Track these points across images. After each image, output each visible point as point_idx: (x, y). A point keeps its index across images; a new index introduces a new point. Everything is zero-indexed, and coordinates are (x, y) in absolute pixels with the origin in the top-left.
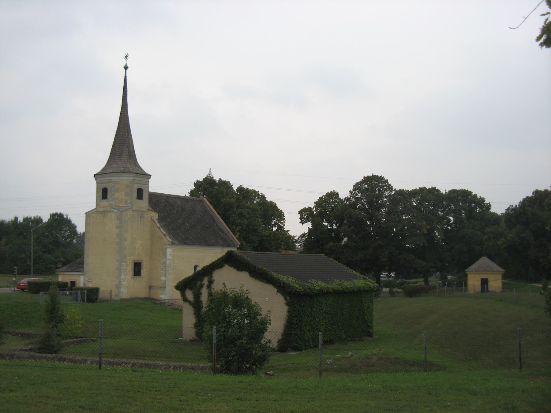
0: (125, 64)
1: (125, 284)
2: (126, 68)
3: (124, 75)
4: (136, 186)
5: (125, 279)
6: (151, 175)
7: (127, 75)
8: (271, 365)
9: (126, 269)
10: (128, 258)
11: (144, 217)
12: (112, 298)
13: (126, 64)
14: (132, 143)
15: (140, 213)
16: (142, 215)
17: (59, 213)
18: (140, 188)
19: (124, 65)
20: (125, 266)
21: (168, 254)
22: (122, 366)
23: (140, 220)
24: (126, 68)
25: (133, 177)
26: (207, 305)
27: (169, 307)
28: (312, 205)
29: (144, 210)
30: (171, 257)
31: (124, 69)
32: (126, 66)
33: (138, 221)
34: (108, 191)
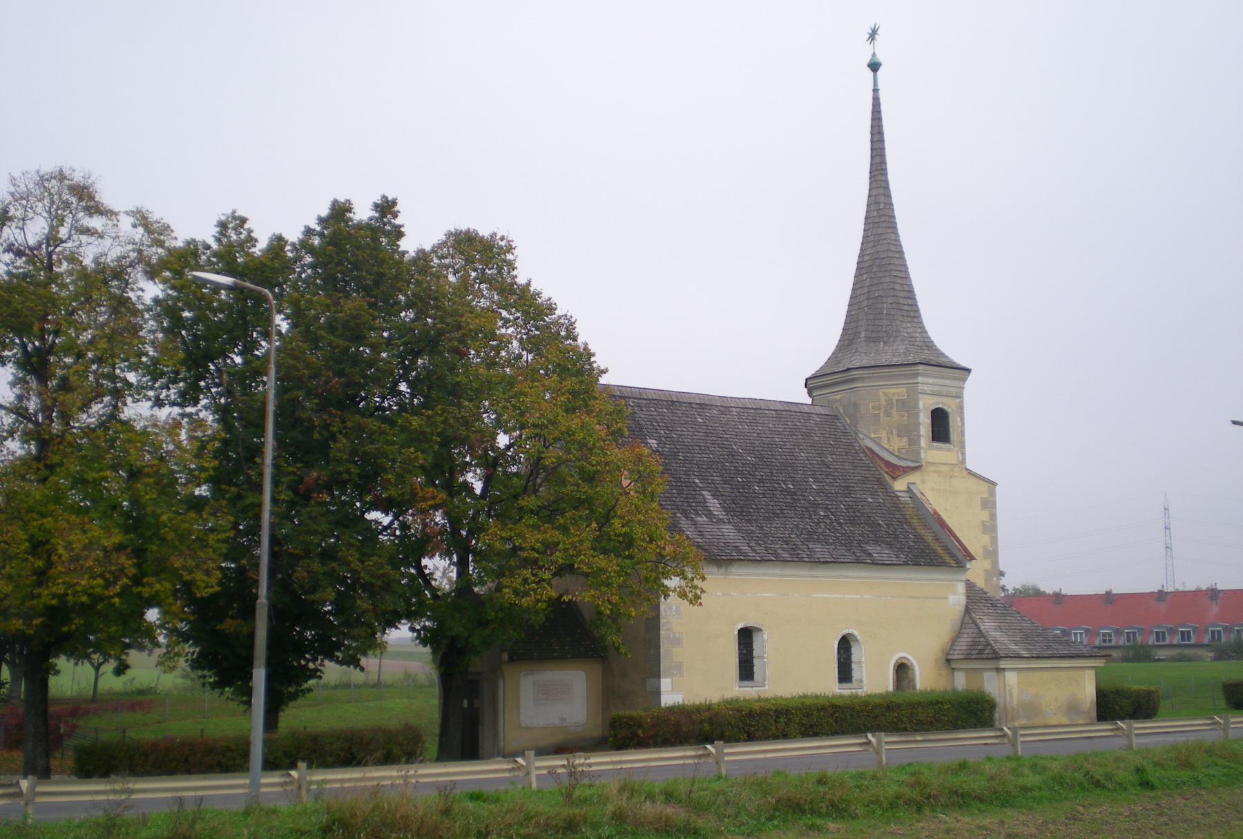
2: (874, 66)
4: (926, 404)
6: (969, 371)
7: (880, 86)
8: (480, 480)
12: (382, 677)
13: (874, 55)
14: (893, 237)
19: (867, 60)
24: (874, 66)
26: (305, 686)
27: (314, 514)
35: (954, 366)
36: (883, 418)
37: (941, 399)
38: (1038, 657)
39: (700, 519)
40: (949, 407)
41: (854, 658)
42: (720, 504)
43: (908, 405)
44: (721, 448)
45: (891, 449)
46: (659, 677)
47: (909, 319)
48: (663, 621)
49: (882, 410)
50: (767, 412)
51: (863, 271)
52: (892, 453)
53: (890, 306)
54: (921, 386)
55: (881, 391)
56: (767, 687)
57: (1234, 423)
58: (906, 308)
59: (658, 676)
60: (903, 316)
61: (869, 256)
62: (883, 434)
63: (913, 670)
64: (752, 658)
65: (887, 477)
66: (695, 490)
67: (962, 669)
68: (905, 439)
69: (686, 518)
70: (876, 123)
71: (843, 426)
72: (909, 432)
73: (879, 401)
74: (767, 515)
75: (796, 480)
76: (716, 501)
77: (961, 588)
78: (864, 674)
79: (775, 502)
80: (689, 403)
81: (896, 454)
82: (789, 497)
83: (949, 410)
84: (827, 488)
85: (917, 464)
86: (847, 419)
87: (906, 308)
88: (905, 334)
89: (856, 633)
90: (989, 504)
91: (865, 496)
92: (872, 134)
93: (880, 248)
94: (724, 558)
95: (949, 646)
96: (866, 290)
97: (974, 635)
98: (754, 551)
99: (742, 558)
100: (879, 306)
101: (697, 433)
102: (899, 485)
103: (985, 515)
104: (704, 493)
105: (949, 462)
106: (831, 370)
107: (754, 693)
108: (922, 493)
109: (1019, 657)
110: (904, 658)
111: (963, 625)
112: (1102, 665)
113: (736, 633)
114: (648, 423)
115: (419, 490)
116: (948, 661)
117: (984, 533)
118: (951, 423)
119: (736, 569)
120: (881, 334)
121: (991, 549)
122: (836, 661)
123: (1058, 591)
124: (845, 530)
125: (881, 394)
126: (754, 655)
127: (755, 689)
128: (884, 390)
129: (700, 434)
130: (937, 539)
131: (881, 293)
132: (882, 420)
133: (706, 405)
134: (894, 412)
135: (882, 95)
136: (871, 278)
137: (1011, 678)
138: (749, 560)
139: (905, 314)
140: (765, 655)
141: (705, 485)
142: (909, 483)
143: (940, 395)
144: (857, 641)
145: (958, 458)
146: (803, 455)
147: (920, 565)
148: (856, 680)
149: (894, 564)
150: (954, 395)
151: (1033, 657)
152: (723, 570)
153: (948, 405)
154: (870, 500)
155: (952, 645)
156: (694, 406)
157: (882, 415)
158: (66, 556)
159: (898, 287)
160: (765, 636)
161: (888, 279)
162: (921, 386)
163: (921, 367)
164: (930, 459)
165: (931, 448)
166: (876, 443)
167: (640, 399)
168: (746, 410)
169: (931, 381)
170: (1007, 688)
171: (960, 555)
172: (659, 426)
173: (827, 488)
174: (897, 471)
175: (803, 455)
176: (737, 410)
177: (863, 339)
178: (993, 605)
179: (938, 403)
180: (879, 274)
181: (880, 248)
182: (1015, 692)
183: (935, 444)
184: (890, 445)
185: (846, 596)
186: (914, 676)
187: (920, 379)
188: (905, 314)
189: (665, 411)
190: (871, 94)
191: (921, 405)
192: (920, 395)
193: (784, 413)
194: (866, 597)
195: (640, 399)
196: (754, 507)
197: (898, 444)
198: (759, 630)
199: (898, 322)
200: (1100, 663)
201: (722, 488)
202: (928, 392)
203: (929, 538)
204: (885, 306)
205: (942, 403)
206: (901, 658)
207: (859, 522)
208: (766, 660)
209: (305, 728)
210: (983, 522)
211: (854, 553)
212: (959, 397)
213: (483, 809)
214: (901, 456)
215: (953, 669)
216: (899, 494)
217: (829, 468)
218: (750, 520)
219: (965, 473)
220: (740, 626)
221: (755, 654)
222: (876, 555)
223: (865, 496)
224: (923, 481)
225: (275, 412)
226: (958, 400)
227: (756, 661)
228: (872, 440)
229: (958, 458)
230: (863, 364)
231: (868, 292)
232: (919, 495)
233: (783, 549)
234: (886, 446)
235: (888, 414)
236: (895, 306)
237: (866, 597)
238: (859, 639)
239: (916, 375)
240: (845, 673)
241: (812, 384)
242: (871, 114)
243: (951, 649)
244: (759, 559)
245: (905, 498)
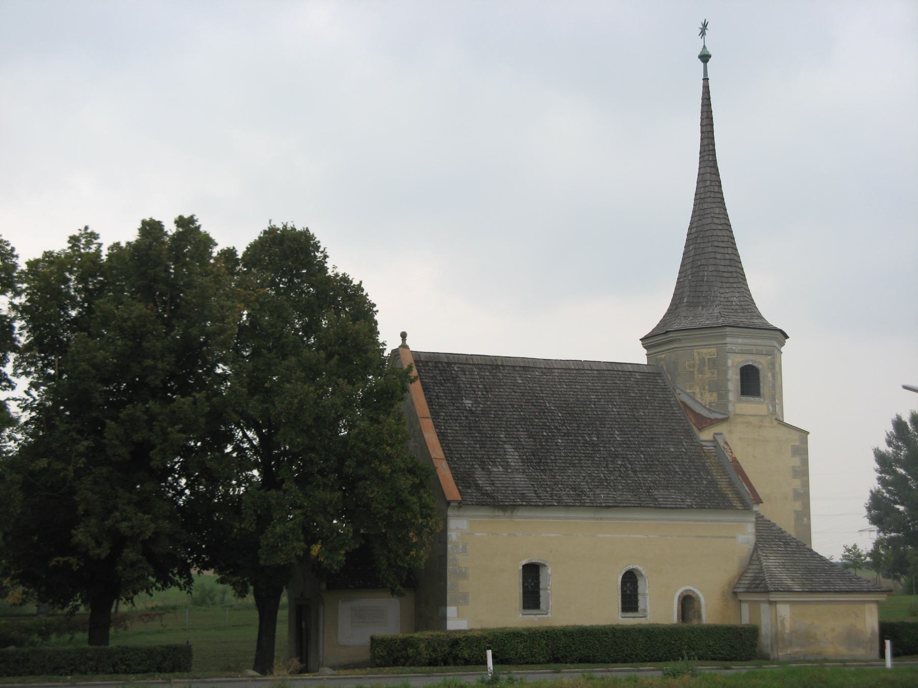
2: (705, 58)
4: (734, 363)
13: (704, 46)
19: (699, 51)
24: (705, 58)
35: (766, 327)
36: (697, 376)
37: (751, 357)
38: (811, 592)
39: (495, 470)
40: (760, 364)
41: (640, 590)
42: (520, 456)
43: (717, 364)
44: (535, 406)
45: (703, 402)
46: (446, 606)
47: (728, 285)
48: (449, 557)
49: (696, 368)
50: (589, 372)
51: (691, 242)
52: (704, 407)
53: (710, 274)
54: (729, 346)
55: (695, 351)
56: (549, 615)
57: (905, 387)
58: (726, 275)
59: (444, 603)
60: (722, 282)
61: (695, 229)
62: (697, 390)
63: (699, 601)
64: (539, 589)
65: (695, 428)
66: (498, 444)
67: (746, 601)
68: (715, 394)
69: (483, 469)
70: (706, 109)
71: (664, 383)
72: (719, 388)
73: (694, 360)
74: (563, 465)
75: (601, 433)
76: (516, 453)
77: (750, 528)
78: (648, 604)
79: (575, 453)
80: (512, 366)
81: (708, 407)
82: (590, 449)
83: (760, 367)
84: (632, 439)
85: (725, 416)
86: (668, 376)
87: (726, 275)
88: (722, 299)
89: (640, 568)
90: (801, 451)
91: (668, 446)
92: (702, 119)
93: (704, 221)
94: (506, 503)
95: (736, 580)
96: (691, 259)
97: (757, 571)
98: (539, 497)
99: (524, 503)
100: (701, 274)
101: (513, 394)
102: (705, 436)
103: (796, 461)
104: (506, 446)
105: (761, 414)
107: (536, 619)
108: (726, 443)
109: (790, 591)
110: (690, 590)
111: (751, 561)
112: (884, 599)
113: (521, 568)
114: (468, 386)
116: (735, 593)
117: (794, 477)
118: (761, 379)
119: (520, 513)
120: (701, 299)
121: (802, 491)
122: (620, 593)
124: (638, 477)
125: (696, 354)
126: (541, 587)
127: (538, 616)
128: (698, 350)
129: (517, 394)
130: (731, 484)
131: (703, 262)
132: (696, 377)
133: (529, 367)
134: (706, 369)
136: (695, 248)
137: (784, 610)
138: (531, 505)
139: (724, 280)
140: (549, 587)
141: (508, 439)
142: (715, 434)
143: (750, 353)
144: (642, 575)
145: (768, 410)
146: (614, 410)
147: (705, 508)
148: (641, 610)
149: (677, 508)
150: (764, 353)
151: (804, 591)
152: (508, 514)
153: (760, 362)
154: (672, 450)
155: (740, 579)
156: (517, 368)
157: (696, 373)
159: (718, 256)
160: (549, 571)
161: (710, 249)
162: (729, 346)
163: (728, 329)
164: (738, 411)
165: (739, 401)
166: (690, 396)
167: (465, 364)
168: (568, 371)
169: (740, 341)
170: (779, 619)
171: (749, 498)
172: (478, 388)
173: (632, 439)
174: (704, 422)
175: (614, 410)
176: (560, 371)
177: (685, 304)
178: (786, 544)
179: (748, 361)
180: (702, 245)
181: (704, 221)
182: (788, 624)
183: (744, 398)
184: (702, 400)
185: (631, 536)
186: (700, 607)
187: (728, 340)
188: (724, 280)
189: (488, 374)
191: (730, 362)
192: (728, 354)
193: (606, 372)
194: (651, 536)
195: (465, 364)
196: (553, 458)
197: (709, 398)
198: (544, 566)
199: (716, 288)
200: (882, 598)
201: (526, 441)
202: (737, 351)
203: (723, 484)
204: (706, 273)
205: (752, 361)
206: (686, 591)
207: (655, 470)
208: (549, 592)
209: (188, 642)
210: (793, 467)
211: (639, 498)
212: (771, 355)
214: (713, 409)
215: (740, 601)
216: (704, 444)
217: (638, 421)
218: (545, 469)
219: (775, 423)
220: (524, 562)
221: (541, 586)
222: (661, 499)
223: (668, 446)
224: (730, 432)
226: (769, 357)
227: (542, 593)
228: (687, 394)
229: (768, 410)
230: (680, 327)
231: (693, 261)
232: (722, 444)
233: (568, 495)
234: (700, 400)
235: (701, 372)
236: (715, 273)
237: (651, 536)
238: (643, 572)
239: (724, 336)
240: (630, 602)
241: (649, 341)
243: (738, 583)
244: (541, 504)
245: (709, 447)
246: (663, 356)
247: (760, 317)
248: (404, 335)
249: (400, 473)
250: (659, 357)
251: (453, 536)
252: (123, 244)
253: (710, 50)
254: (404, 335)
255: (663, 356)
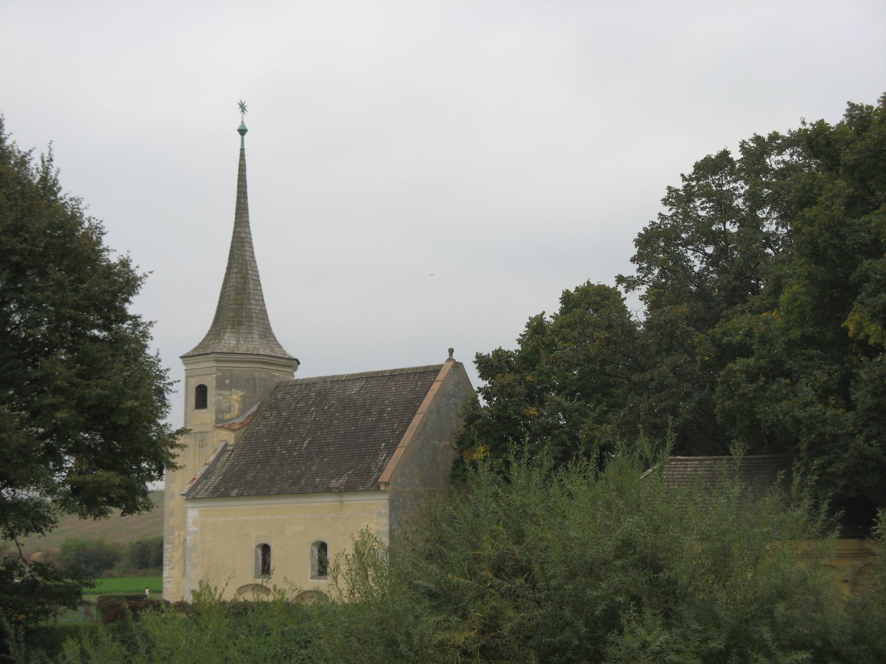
0: (241, 122)
1: (170, 588)
2: (243, 131)
3: (239, 147)
5: (171, 578)
7: (245, 147)
9: (172, 556)
10: (177, 533)
11: (206, 444)
13: (243, 122)
15: (198, 438)
16: (203, 441)
17: (551, 308)
18: (201, 383)
19: (238, 125)
20: (171, 550)
21: (190, 520)
22: (808, 459)
23: (199, 452)
24: (243, 131)
25: (217, 361)
28: (560, 305)
29: (208, 429)
30: (196, 529)
31: (238, 133)
32: (243, 128)
33: (195, 457)
34: (208, 390)
106: (196, 353)
115: (55, 525)
123: (180, 599)
135: (246, 152)
158: (820, 407)
190: (239, 151)
213: (160, 383)
225: (391, 449)
242: (237, 171)
246: (277, 374)
247: (279, 346)
248: (451, 351)
249: (552, 431)
250: (272, 373)
251: (385, 521)
252: (572, 290)
253: (247, 126)
254: (451, 351)
255: (277, 374)
